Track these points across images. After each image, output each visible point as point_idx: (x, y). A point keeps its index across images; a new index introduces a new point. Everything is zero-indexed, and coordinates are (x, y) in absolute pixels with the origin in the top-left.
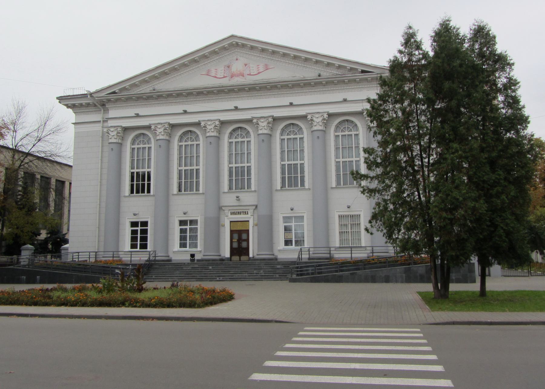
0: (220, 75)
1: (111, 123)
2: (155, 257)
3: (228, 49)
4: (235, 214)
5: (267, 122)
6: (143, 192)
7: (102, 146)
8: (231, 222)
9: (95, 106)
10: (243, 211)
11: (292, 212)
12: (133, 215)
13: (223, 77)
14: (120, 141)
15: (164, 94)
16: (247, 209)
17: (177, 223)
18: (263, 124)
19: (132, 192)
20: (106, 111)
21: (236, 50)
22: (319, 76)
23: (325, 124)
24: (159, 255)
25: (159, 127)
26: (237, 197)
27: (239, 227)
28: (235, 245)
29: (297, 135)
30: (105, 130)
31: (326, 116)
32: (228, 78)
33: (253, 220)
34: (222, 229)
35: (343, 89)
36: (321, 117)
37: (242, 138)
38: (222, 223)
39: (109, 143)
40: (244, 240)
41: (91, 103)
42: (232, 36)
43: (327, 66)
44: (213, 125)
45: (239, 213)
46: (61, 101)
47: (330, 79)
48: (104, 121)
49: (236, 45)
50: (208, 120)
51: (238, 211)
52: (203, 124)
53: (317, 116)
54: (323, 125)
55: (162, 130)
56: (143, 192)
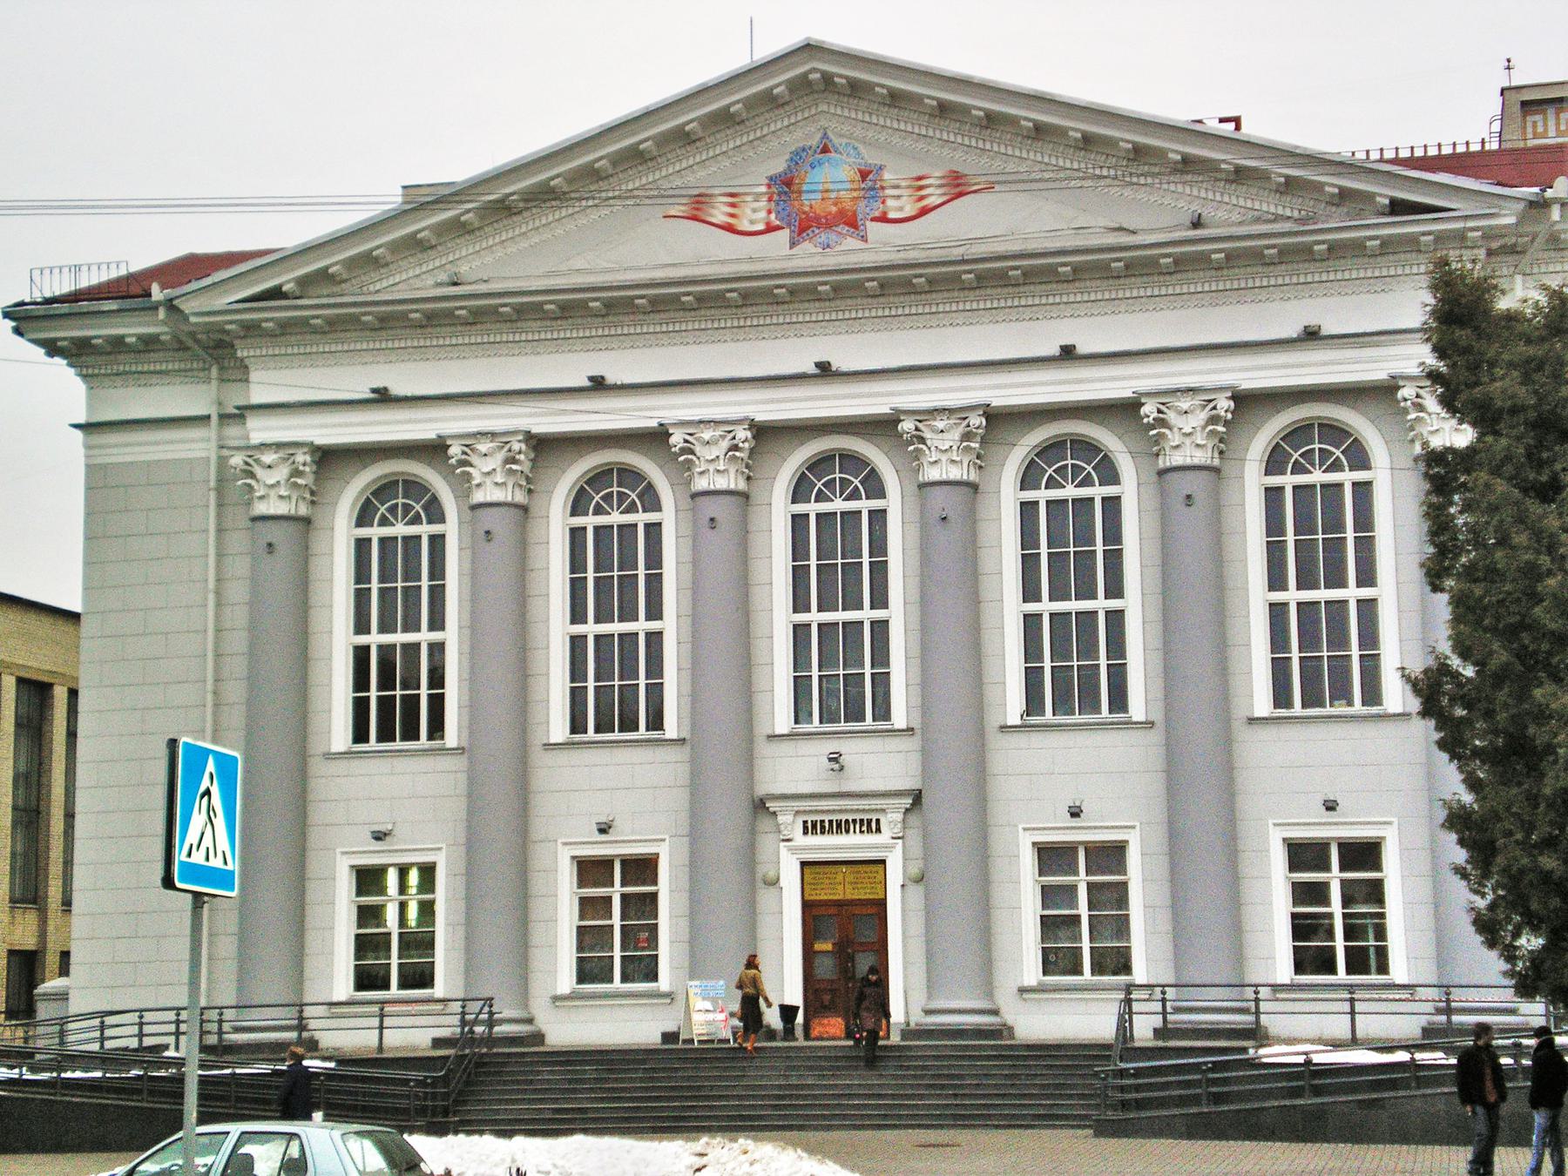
0: (752, 222)
1: (261, 430)
2: (491, 1023)
3: (787, 103)
4: (823, 833)
5: (961, 429)
6: (411, 733)
7: (220, 531)
8: (804, 864)
9: (182, 347)
10: (858, 817)
11: (1075, 822)
12: (595, 828)
13: (761, 227)
14: (303, 510)
15: (267, 320)
16: (876, 810)
17: (1028, 861)
18: (944, 438)
19: (360, 735)
20: (238, 372)
21: (824, 107)
22: (1197, 224)
23: (1221, 441)
24: (507, 1014)
25: (483, 447)
26: (835, 758)
27: (841, 889)
28: (826, 968)
29: (1093, 485)
30: (237, 460)
31: (1224, 404)
32: (784, 235)
33: (905, 859)
34: (765, 897)
35: (286, 355)
36: (723, 437)
37: (626, 511)
38: (765, 869)
39: (255, 519)
40: (866, 948)
41: (163, 338)
42: (810, 49)
43: (1233, 182)
44: (725, 444)
45: (841, 827)
46: (24, 326)
47: (944, 269)
48: (224, 417)
49: (822, 87)
50: (701, 422)
51: (834, 817)
52: (677, 439)
53: (1185, 404)
54: (1210, 446)
55: (495, 462)
56: (411, 733)
